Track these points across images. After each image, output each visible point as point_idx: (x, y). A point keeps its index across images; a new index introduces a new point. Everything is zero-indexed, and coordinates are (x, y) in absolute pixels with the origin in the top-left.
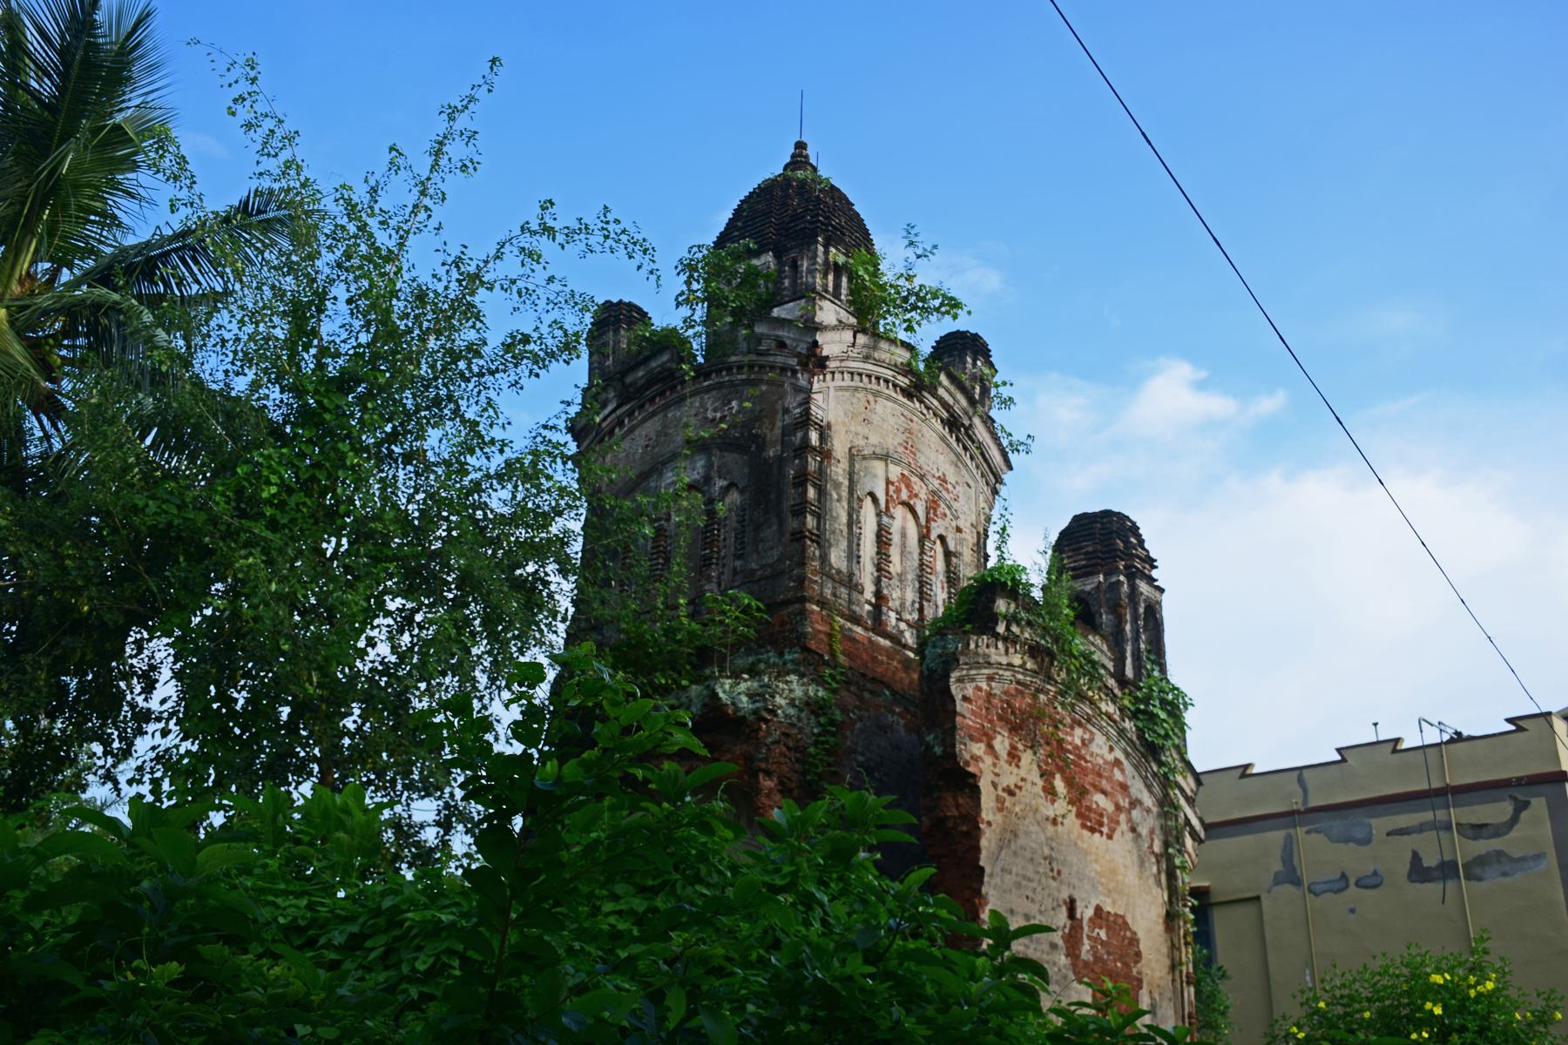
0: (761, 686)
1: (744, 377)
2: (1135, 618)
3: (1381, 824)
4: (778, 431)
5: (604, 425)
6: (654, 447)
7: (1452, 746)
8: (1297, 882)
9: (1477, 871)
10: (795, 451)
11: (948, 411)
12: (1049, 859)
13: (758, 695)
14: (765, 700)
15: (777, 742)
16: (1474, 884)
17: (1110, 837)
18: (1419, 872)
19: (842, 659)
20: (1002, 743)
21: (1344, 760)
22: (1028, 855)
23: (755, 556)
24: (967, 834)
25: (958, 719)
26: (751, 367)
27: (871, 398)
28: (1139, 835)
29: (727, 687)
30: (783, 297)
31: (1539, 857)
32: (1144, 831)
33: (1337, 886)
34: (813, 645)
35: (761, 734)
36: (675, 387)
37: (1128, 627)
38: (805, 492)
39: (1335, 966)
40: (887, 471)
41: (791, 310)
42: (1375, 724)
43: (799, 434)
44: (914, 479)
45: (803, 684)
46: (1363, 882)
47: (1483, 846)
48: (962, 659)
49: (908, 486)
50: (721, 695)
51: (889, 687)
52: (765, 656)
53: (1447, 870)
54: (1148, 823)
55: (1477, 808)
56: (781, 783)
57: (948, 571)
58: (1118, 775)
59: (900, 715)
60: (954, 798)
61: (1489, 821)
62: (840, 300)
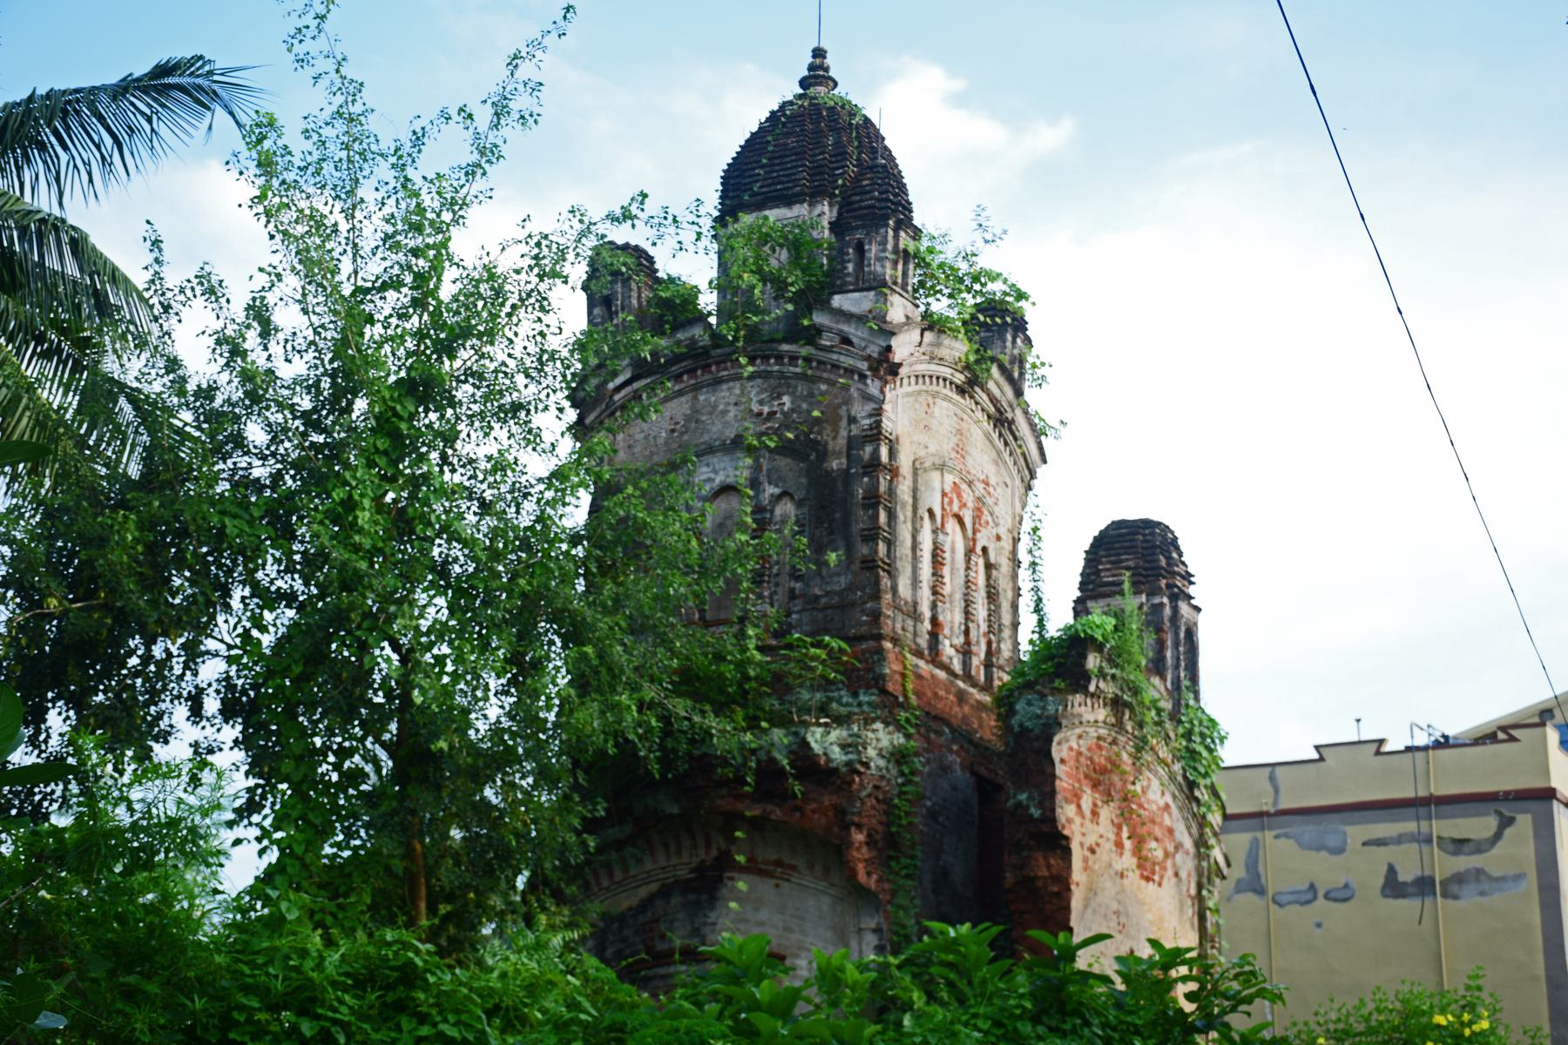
0: (850, 736)
1: (798, 370)
2: (1176, 644)
3: (1357, 832)
4: (842, 442)
5: (616, 397)
6: (682, 434)
7: (1441, 753)
8: (1260, 891)
9: (1454, 888)
10: (864, 467)
11: (995, 406)
12: (1117, 913)
13: (849, 745)
14: (859, 753)
15: (869, 796)
16: (1450, 902)
17: (1160, 885)
18: (1393, 887)
19: (913, 700)
20: (1086, 803)
21: (1322, 759)
22: (1103, 911)
23: (818, 580)
24: (1057, 895)
25: (1058, 783)
26: (807, 360)
27: (931, 401)
28: (1180, 880)
29: (818, 736)
30: (846, 284)
31: (1519, 877)
32: (1183, 874)
33: (1304, 898)
34: (890, 687)
35: (855, 787)
36: (709, 366)
37: (1169, 654)
38: (877, 516)
39: (1332, 1000)
40: (942, 482)
41: (857, 302)
42: (1358, 721)
43: (869, 449)
44: (964, 486)
45: (889, 733)
46: (1332, 895)
47: (1464, 863)
48: (1064, 722)
49: (959, 496)
50: (813, 745)
51: (948, 724)
52: (836, 694)
53: (1424, 886)
54: (1186, 863)
55: (1459, 821)
56: (869, 835)
57: (988, 586)
58: (1167, 821)
59: (957, 753)
60: (1045, 858)
61: (1471, 836)
62: (907, 292)
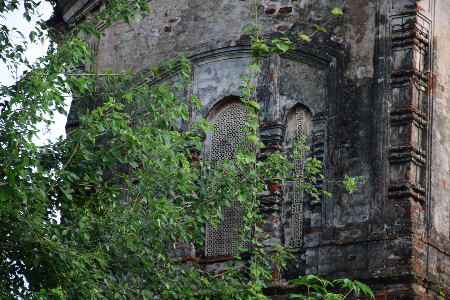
10: (393, 76)
23: (337, 210)
43: (400, 54)
